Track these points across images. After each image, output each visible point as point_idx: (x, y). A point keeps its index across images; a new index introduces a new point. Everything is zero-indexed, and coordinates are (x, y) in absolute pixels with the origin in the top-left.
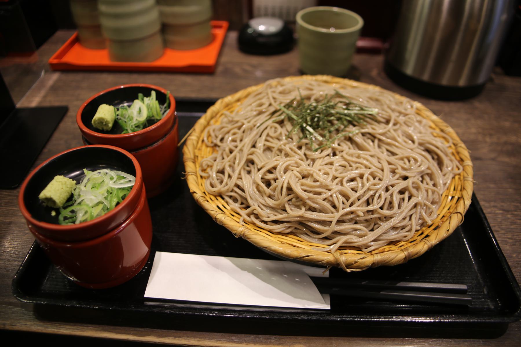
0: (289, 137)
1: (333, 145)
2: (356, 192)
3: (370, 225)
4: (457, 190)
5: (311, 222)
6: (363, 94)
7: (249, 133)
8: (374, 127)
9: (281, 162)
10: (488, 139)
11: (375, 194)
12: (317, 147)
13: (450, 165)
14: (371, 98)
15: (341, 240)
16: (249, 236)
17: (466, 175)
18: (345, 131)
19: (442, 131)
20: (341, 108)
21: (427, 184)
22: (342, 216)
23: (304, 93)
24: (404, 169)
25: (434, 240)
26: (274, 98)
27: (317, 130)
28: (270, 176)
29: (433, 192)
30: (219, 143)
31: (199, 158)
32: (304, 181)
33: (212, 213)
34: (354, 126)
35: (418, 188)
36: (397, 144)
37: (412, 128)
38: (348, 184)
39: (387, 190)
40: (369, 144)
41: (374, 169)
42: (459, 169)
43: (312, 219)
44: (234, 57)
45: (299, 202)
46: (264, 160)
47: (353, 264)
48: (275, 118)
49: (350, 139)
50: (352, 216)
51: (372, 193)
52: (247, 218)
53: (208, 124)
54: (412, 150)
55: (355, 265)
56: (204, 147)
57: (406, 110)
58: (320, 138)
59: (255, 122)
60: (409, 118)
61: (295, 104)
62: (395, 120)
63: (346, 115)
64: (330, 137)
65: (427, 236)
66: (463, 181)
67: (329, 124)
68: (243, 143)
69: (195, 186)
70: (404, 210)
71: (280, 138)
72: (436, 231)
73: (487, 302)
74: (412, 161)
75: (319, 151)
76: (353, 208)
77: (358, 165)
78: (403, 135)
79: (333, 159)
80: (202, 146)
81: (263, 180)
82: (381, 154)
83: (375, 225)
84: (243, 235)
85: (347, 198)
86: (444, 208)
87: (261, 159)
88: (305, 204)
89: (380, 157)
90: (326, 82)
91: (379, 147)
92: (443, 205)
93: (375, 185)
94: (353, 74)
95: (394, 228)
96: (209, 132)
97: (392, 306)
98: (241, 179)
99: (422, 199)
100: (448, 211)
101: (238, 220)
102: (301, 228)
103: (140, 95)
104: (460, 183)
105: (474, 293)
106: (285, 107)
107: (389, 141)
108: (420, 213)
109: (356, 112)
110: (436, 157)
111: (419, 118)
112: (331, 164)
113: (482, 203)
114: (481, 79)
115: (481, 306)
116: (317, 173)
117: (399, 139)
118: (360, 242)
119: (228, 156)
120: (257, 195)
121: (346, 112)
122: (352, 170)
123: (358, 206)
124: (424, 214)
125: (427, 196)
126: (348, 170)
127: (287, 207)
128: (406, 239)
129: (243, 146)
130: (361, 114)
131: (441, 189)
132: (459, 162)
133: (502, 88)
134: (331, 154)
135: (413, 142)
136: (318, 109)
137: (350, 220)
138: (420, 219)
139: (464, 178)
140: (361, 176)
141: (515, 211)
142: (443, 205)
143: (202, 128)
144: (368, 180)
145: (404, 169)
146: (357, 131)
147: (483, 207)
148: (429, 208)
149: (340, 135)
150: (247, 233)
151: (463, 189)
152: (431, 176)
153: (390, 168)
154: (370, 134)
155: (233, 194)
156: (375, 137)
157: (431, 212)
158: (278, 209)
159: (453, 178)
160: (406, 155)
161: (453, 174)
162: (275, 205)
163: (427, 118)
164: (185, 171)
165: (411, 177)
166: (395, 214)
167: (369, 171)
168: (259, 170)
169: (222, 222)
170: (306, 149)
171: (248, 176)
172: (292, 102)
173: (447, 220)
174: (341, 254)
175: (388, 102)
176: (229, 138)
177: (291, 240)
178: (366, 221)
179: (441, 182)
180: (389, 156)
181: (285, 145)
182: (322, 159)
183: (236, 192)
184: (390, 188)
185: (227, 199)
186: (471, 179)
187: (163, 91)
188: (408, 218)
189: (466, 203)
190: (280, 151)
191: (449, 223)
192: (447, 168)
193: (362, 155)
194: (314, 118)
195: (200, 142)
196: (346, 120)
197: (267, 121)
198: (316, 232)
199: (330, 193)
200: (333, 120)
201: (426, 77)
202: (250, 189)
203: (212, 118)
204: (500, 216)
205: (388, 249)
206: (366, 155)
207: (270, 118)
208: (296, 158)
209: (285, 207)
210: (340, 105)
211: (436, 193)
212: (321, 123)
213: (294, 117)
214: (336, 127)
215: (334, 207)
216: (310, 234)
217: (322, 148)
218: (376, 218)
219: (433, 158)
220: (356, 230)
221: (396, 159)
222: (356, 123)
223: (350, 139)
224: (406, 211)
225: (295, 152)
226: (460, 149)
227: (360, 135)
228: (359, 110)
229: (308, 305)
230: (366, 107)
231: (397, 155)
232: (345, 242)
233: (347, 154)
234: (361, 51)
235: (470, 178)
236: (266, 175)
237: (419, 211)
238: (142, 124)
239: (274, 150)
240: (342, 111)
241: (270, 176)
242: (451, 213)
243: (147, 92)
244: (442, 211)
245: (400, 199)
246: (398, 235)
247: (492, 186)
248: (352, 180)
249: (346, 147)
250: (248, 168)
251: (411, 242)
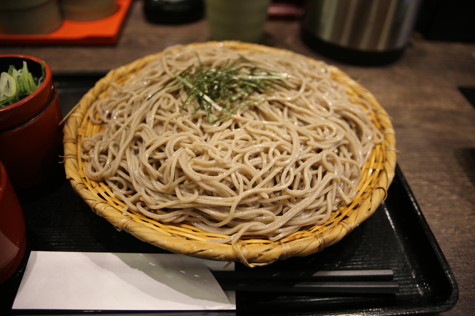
0: (184, 109)
1: (235, 116)
2: (261, 169)
3: (277, 208)
4: (378, 162)
5: (206, 208)
6: (272, 61)
7: (138, 106)
8: (283, 93)
9: (172, 138)
10: (410, 106)
11: (283, 171)
12: (216, 118)
13: (370, 134)
14: (280, 63)
15: (244, 228)
16: (132, 229)
17: (387, 144)
18: (250, 99)
19: (361, 96)
20: (245, 75)
21: (345, 156)
22: (243, 199)
23: (204, 59)
24: (316, 140)
25: (353, 222)
26: (169, 66)
27: (217, 100)
28: (159, 156)
29: (351, 166)
30: (105, 120)
31: (83, 138)
32: (198, 160)
33: (90, 202)
34: (260, 93)
35: (333, 162)
36: (309, 112)
37: (327, 94)
38: (251, 161)
39: (297, 165)
40: (277, 113)
41: (281, 141)
42: (380, 138)
43: (207, 205)
44: (139, 27)
45: (190, 185)
46: (152, 137)
47: (256, 258)
48: (170, 87)
49: (256, 109)
50: (256, 199)
51: (278, 170)
52: (133, 207)
53: (97, 98)
54: (326, 118)
55: (260, 258)
56: (90, 125)
57: (319, 73)
58: (220, 109)
59: (147, 93)
60: (324, 83)
61: (193, 72)
62: (307, 85)
63: (250, 81)
64: (232, 107)
65: (346, 217)
66: (384, 151)
67: (231, 92)
68: (131, 118)
69: (72, 171)
70: (317, 189)
71: (174, 110)
72: (356, 211)
73: (416, 287)
74: (327, 131)
75: (218, 123)
76: (257, 189)
77: (263, 137)
78: (316, 102)
79: (234, 131)
80: (87, 124)
81: (151, 161)
82: (291, 124)
83: (284, 207)
84: (126, 228)
85: (249, 177)
86: (364, 183)
87: (150, 136)
88: (198, 188)
89: (289, 127)
90: (234, 48)
91: (289, 116)
92: (363, 180)
93: (282, 160)
94: (267, 40)
95: (306, 211)
96: (95, 108)
97: (307, 300)
98: (126, 160)
99: (338, 174)
100: (369, 187)
101: (121, 210)
102: (194, 216)
104: (381, 153)
105: (401, 278)
106: (180, 75)
107: (301, 109)
108: (337, 190)
109: (261, 77)
110: (354, 125)
111: (335, 84)
112: (232, 138)
113: (406, 174)
114: (400, 43)
115: (409, 293)
116: (212, 150)
117: (311, 106)
118: (264, 228)
119: (113, 133)
120: (145, 181)
121: (250, 77)
122: (256, 144)
123: (263, 187)
124: (341, 192)
125: (345, 170)
126: (252, 144)
127: (178, 191)
128: (321, 222)
129: (131, 122)
130: (268, 80)
131: (361, 162)
132: (380, 130)
133: (422, 53)
134: (233, 127)
135: (328, 109)
136: (217, 76)
137: (254, 204)
138: (336, 197)
139: (386, 147)
140: (266, 151)
141: (442, 181)
142: (363, 180)
143: (89, 103)
144: (274, 154)
145: (316, 140)
146: (263, 99)
147: (408, 180)
148: (347, 184)
149: (243, 104)
150: (130, 225)
151: (385, 160)
152: (349, 147)
153: (300, 140)
154: (278, 102)
155: (115, 178)
156: (284, 105)
157: (350, 189)
158: (168, 194)
159: (374, 148)
160: (320, 124)
161: (374, 143)
162: (163, 189)
163: (344, 83)
164: (63, 154)
165: (325, 149)
166: (307, 193)
167: (275, 144)
168: (148, 148)
169: (101, 213)
170: (202, 123)
171: (134, 156)
172: (190, 68)
173: (368, 197)
174: (243, 246)
175: (299, 66)
176: (116, 113)
177: (185, 231)
178: (274, 203)
179: (360, 153)
180: (300, 126)
181: (176, 119)
182: (221, 133)
183: (121, 177)
184: (301, 163)
185: (111, 185)
187: (35, 60)
188: (323, 198)
189: (389, 176)
190: (172, 124)
191: (371, 201)
192: (367, 136)
193: (267, 126)
194: (214, 86)
195: (85, 120)
196: (250, 87)
197: (159, 91)
198: (214, 220)
199: (228, 172)
200: (236, 87)
201: (344, 42)
202: (135, 170)
203: (101, 91)
204: (426, 188)
205: (299, 236)
206: (273, 125)
207: (162, 89)
208: (190, 133)
209: (174, 191)
210: (244, 70)
211: (355, 167)
212: (221, 92)
213: (190, 86)
214: (239, 95)
215: (234, 189)
216: (207, 223)
217: (221, 120)
218: (284, 200)
219: (351, 127)
220: (261, 215)
221: (308, 129)
222: (262, 90)
223: (256, 109)
224: (320, 189)
225: (190, 126)
226: (381, 117)
227: (267, 103)
228: (266, 75)
229: (210, 306)
230: (274, 72)
231: (309, 124)
232: (249, 231)
233: (250, 125)
234: (273, 18)
235: (392, 148)
236: (155, 155)
237: (335, 188)
239: (166, 124)
240: (246, 77)
241: (159, 156)
242: (372, 189)
244: (362, 186)
245: (313, 175)
246: (311, 219)
247: (416, 155)
248: (257, 155)
249: (251, 118)
250: (136, 147)
251: (326, 226)
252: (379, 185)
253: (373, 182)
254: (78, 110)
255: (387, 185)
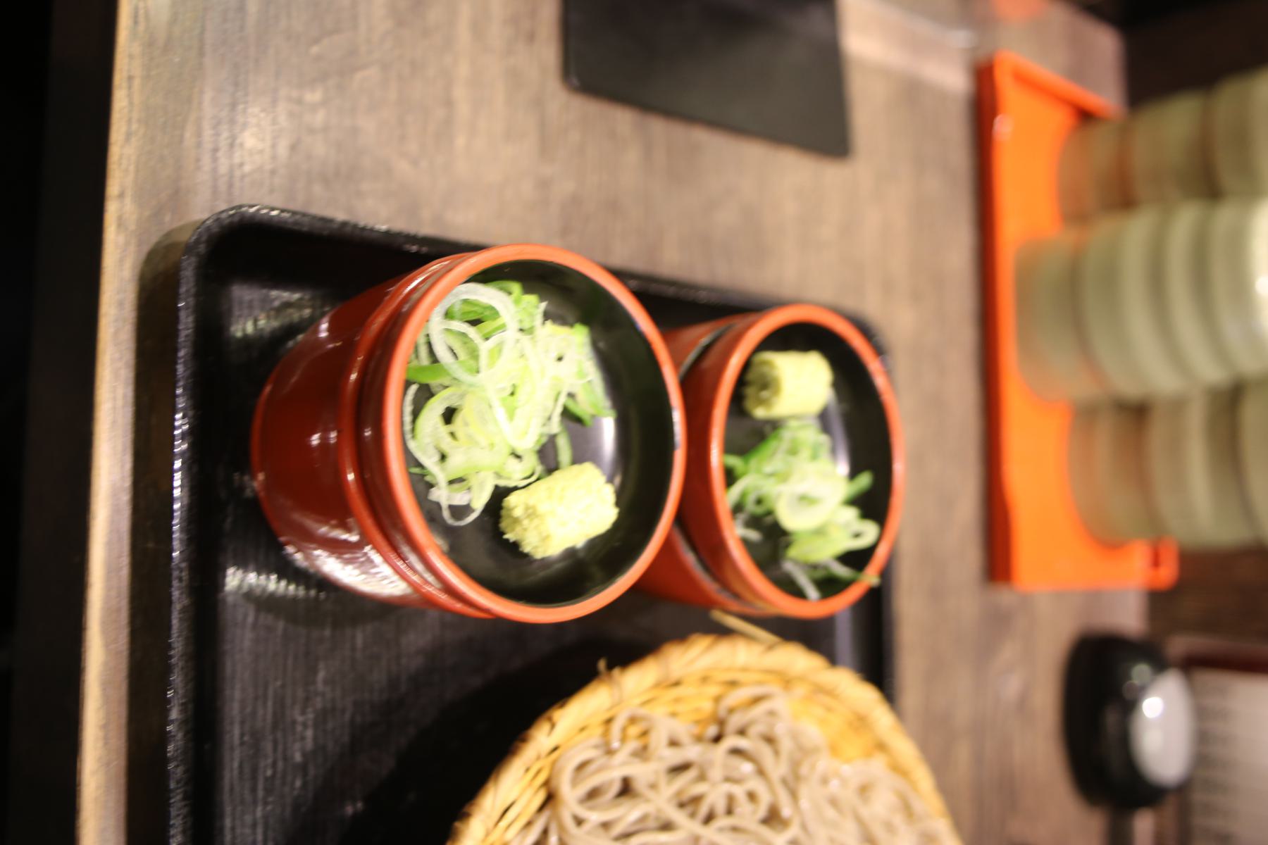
56: (713, 690)
103: (865, 480)
238: (770, 513)
243: (873, 504)
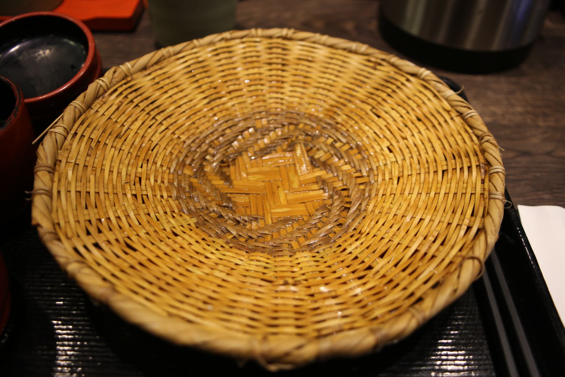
31: (63, 164)
33: (61, 260)
53: (89, 107)
72: (435, 291)
86: (452, 247)
139: (490, 194)
151: (486, 213)
186: (500, 197)
191: (459, 277)
201: (440, 39)
252: (473, 253)
253: (465, 246)
254: (60, 124)
255: (485, 255)
